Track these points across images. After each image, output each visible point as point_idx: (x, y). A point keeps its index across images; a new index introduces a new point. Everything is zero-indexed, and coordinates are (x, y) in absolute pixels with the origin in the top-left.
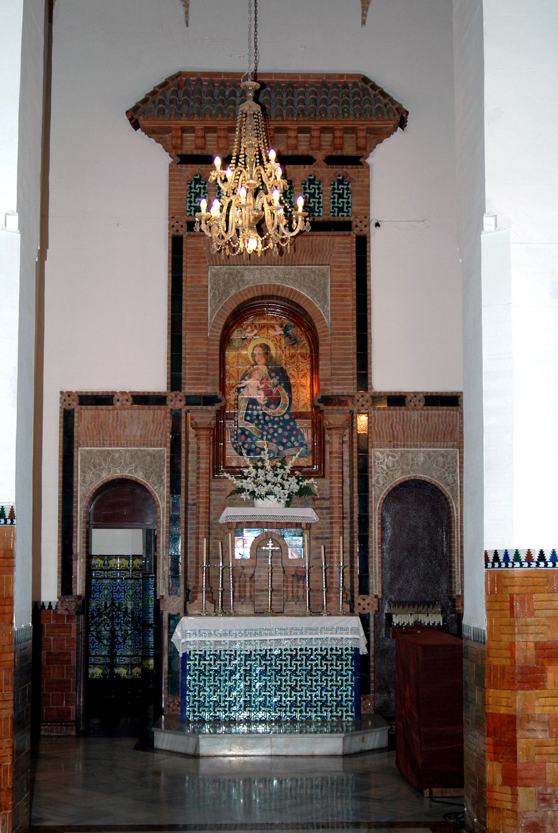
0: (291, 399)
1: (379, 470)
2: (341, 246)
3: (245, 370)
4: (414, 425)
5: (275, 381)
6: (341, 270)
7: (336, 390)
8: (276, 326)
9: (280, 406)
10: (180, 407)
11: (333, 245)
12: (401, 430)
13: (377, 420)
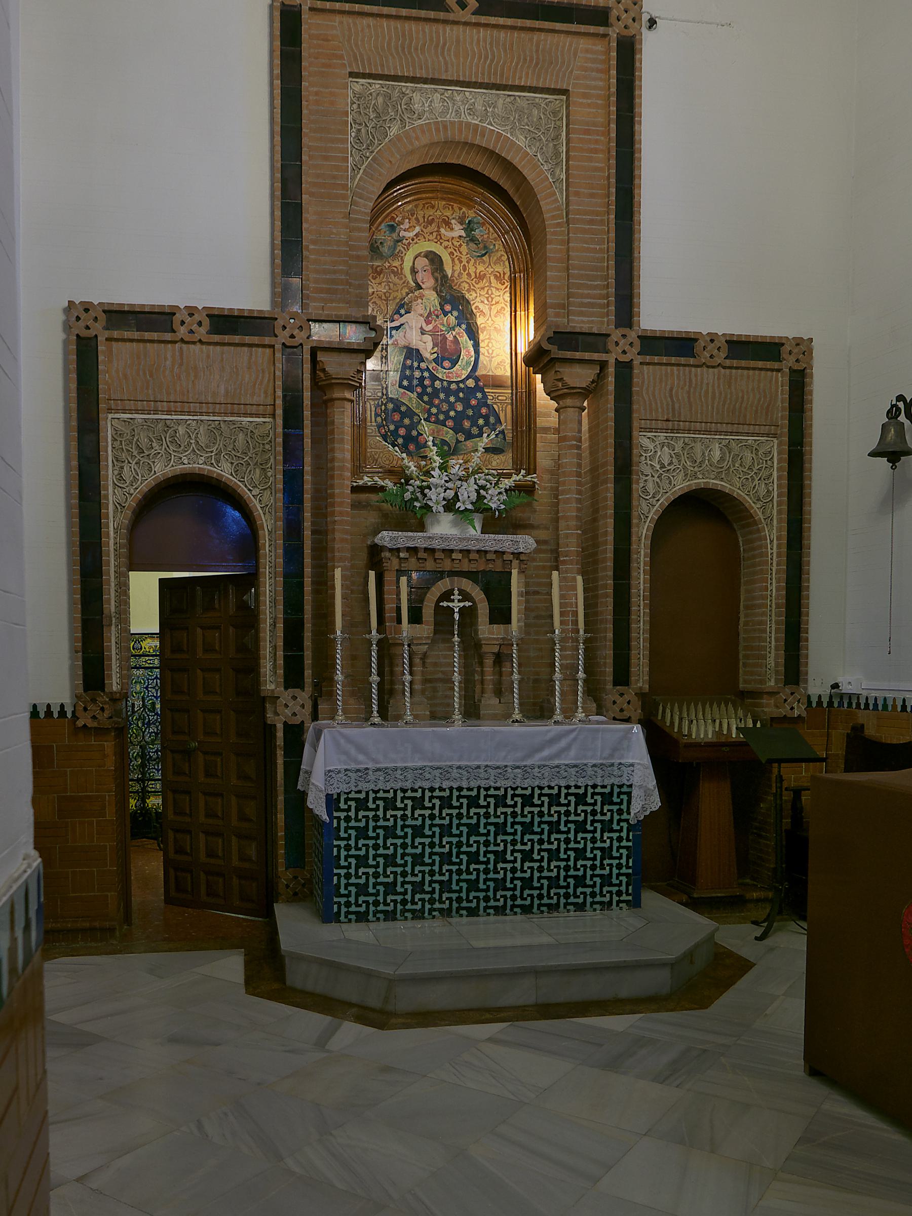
0: (477, 352)
1: (648, 471)
2: (589, 56)
3: (400, 296)
4: (707, 392)
5: (452, 319)
6: (589, 101)
7: (581, 323)
8: (453, 221)
9: (459, 363)
10: (301, 341)
11: (575, 55)
12: (686, 400)
13: (646, 382)
